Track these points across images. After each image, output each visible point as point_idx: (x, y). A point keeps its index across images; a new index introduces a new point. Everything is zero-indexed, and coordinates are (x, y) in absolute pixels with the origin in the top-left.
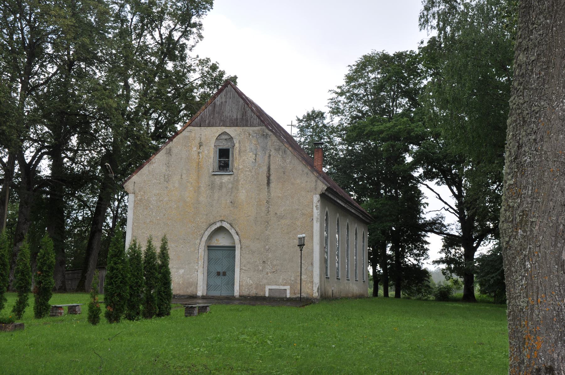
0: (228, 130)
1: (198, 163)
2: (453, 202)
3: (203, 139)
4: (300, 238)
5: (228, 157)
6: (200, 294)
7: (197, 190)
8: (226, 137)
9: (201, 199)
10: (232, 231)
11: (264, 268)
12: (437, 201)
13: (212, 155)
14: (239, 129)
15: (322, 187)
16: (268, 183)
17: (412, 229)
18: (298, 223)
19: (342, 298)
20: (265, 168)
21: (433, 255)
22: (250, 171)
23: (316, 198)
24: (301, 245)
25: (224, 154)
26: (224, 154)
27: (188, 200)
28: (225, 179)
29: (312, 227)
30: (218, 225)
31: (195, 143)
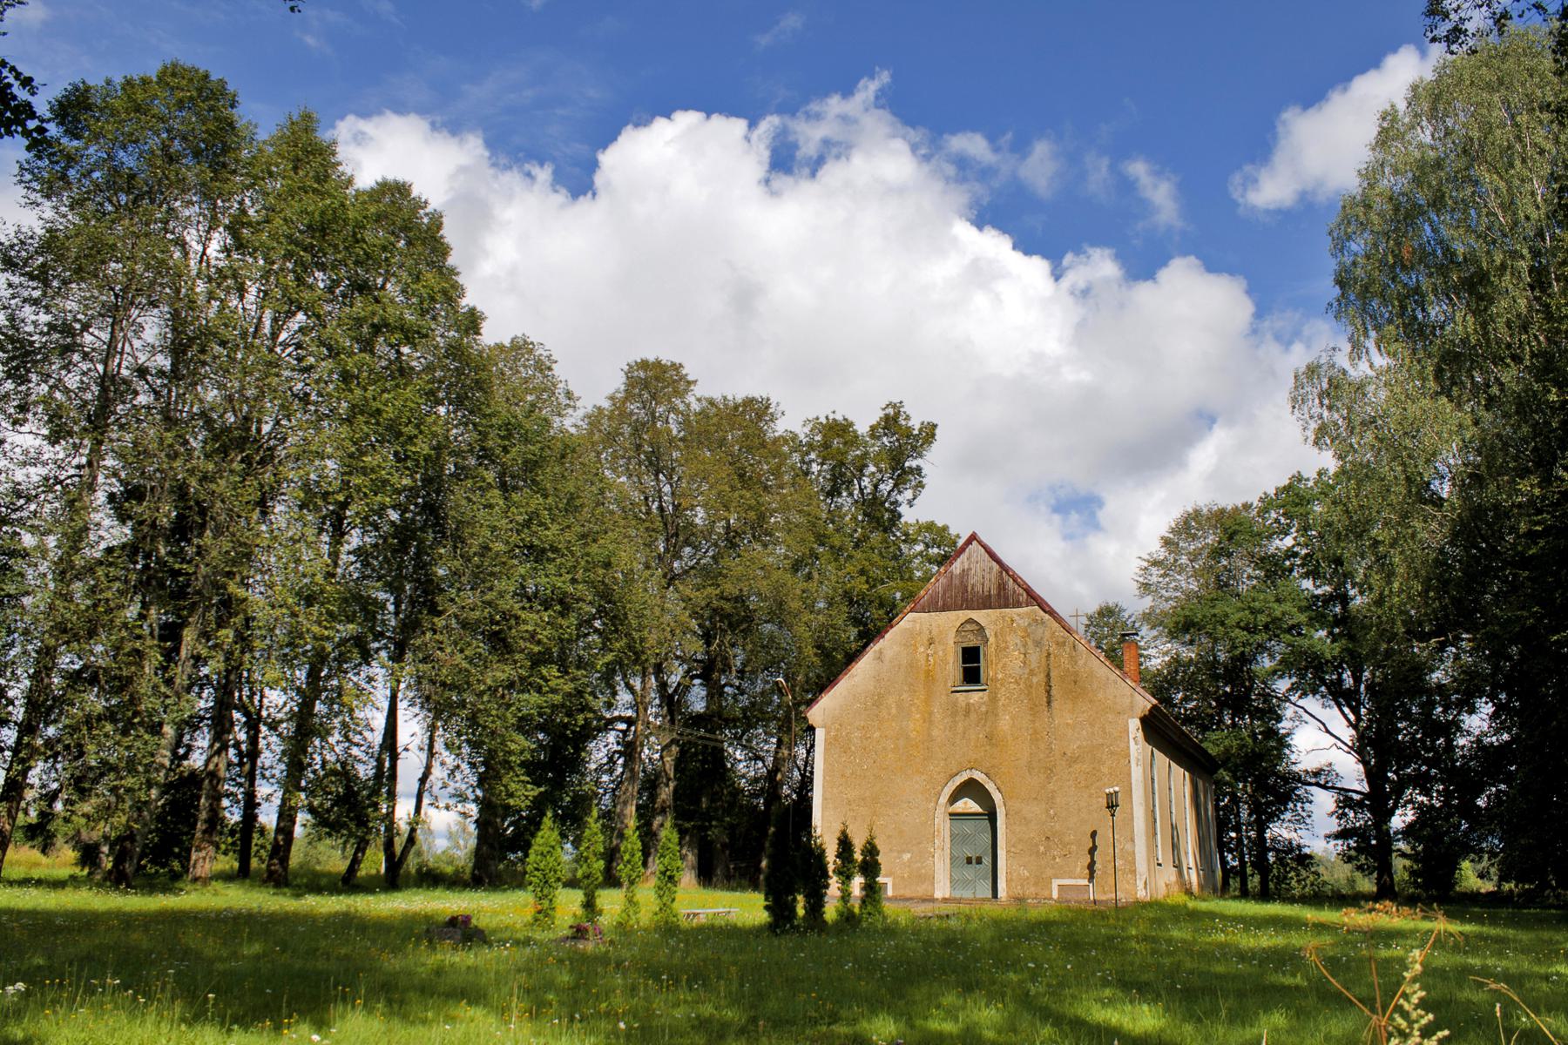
0: (975, 615)
1: (928, 672)
2: (1348, 734)
3: (934, 633)
4: (1109, 795)
5: (965, 669)
6: (938, 895)
7: (928, 719)
8: (974, 627)
9: (935, 733)
10: (990, 787)
11: (1048, 849)
12: (1320, 738)
13: (951, 659)
14: (993, 614)
15: (1145, 702)
16: (1049, 703)
17: (1276, 787)
18: (1105, 770)
19: (211, 878)
20: (1042, 676)
21: (1315, 828)
22: (1017, 683)
23: (1134, 725)
24: (1112, 806)
25: (971, 656)
26: (971, 656)
27: (913, 735)
28: (975, 697)
29: (1129, 775)
30: (964, 777)
31: (920, 637)
